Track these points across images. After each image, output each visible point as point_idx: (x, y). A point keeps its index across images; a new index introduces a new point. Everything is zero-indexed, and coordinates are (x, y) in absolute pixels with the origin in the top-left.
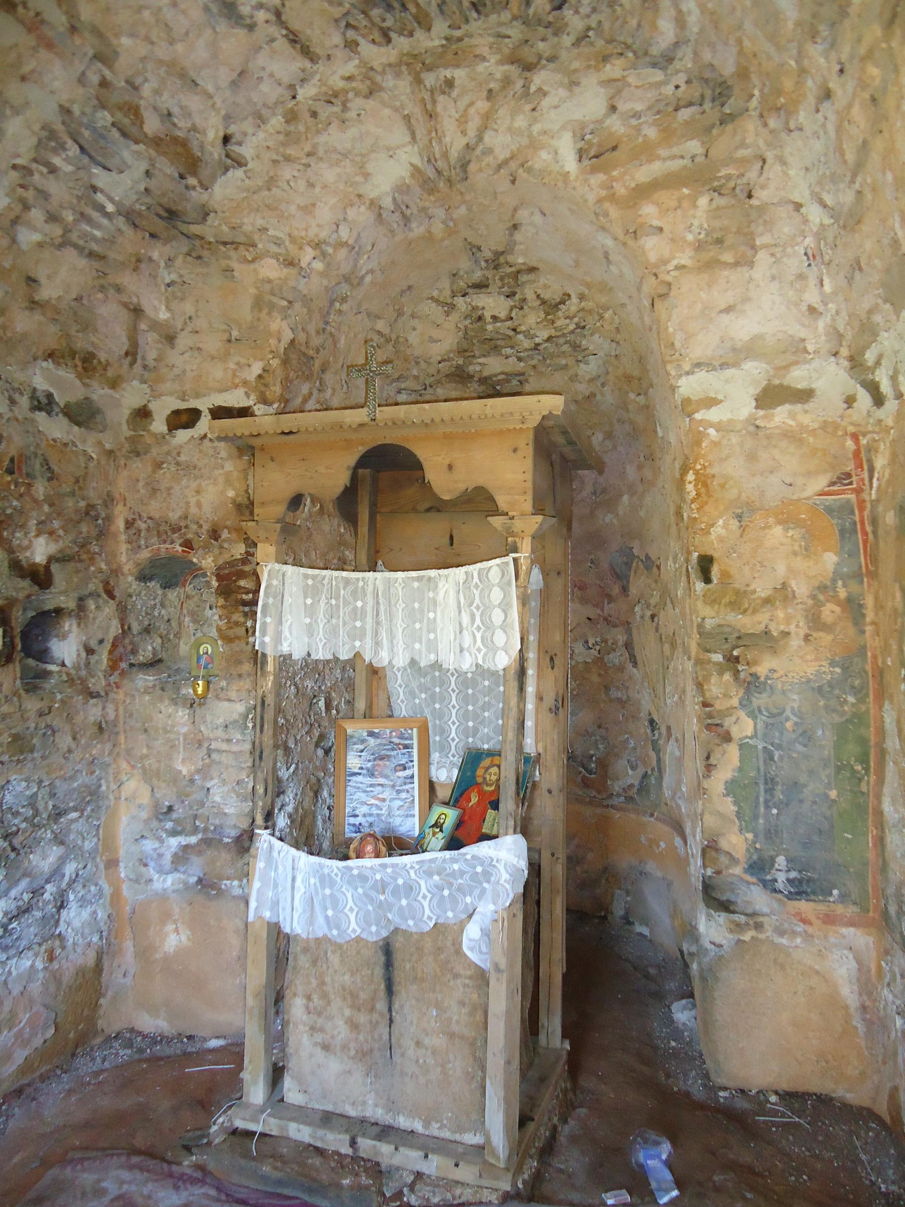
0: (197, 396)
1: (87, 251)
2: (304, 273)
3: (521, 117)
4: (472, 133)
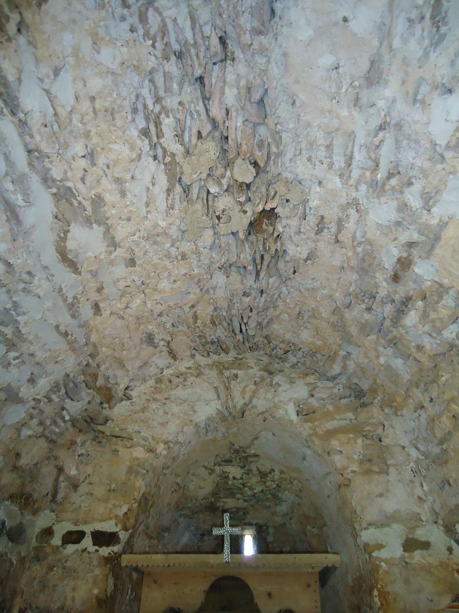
0: (85, 523)
1: (50, 439)
2: (157, 456)
3: (270, 394)
4: (247, 398)
